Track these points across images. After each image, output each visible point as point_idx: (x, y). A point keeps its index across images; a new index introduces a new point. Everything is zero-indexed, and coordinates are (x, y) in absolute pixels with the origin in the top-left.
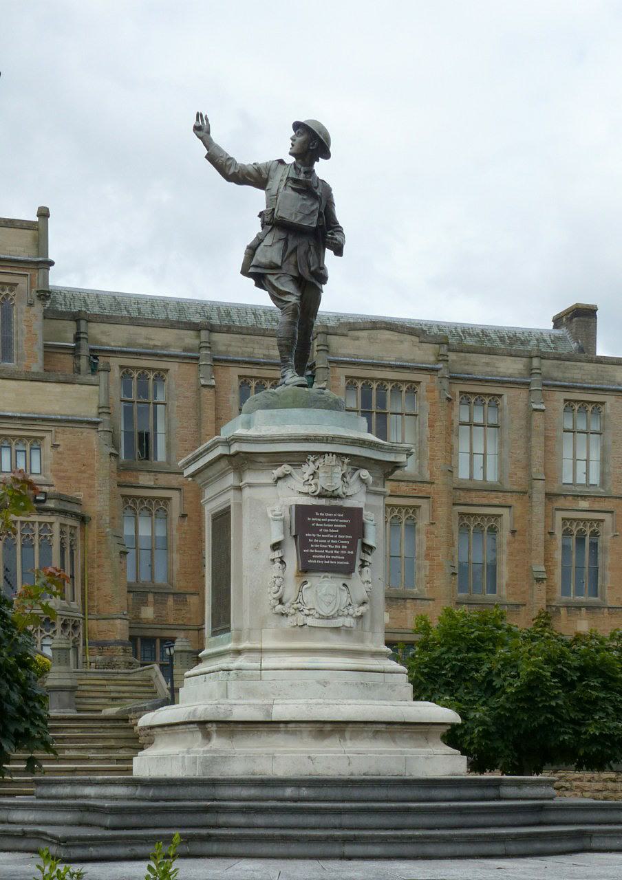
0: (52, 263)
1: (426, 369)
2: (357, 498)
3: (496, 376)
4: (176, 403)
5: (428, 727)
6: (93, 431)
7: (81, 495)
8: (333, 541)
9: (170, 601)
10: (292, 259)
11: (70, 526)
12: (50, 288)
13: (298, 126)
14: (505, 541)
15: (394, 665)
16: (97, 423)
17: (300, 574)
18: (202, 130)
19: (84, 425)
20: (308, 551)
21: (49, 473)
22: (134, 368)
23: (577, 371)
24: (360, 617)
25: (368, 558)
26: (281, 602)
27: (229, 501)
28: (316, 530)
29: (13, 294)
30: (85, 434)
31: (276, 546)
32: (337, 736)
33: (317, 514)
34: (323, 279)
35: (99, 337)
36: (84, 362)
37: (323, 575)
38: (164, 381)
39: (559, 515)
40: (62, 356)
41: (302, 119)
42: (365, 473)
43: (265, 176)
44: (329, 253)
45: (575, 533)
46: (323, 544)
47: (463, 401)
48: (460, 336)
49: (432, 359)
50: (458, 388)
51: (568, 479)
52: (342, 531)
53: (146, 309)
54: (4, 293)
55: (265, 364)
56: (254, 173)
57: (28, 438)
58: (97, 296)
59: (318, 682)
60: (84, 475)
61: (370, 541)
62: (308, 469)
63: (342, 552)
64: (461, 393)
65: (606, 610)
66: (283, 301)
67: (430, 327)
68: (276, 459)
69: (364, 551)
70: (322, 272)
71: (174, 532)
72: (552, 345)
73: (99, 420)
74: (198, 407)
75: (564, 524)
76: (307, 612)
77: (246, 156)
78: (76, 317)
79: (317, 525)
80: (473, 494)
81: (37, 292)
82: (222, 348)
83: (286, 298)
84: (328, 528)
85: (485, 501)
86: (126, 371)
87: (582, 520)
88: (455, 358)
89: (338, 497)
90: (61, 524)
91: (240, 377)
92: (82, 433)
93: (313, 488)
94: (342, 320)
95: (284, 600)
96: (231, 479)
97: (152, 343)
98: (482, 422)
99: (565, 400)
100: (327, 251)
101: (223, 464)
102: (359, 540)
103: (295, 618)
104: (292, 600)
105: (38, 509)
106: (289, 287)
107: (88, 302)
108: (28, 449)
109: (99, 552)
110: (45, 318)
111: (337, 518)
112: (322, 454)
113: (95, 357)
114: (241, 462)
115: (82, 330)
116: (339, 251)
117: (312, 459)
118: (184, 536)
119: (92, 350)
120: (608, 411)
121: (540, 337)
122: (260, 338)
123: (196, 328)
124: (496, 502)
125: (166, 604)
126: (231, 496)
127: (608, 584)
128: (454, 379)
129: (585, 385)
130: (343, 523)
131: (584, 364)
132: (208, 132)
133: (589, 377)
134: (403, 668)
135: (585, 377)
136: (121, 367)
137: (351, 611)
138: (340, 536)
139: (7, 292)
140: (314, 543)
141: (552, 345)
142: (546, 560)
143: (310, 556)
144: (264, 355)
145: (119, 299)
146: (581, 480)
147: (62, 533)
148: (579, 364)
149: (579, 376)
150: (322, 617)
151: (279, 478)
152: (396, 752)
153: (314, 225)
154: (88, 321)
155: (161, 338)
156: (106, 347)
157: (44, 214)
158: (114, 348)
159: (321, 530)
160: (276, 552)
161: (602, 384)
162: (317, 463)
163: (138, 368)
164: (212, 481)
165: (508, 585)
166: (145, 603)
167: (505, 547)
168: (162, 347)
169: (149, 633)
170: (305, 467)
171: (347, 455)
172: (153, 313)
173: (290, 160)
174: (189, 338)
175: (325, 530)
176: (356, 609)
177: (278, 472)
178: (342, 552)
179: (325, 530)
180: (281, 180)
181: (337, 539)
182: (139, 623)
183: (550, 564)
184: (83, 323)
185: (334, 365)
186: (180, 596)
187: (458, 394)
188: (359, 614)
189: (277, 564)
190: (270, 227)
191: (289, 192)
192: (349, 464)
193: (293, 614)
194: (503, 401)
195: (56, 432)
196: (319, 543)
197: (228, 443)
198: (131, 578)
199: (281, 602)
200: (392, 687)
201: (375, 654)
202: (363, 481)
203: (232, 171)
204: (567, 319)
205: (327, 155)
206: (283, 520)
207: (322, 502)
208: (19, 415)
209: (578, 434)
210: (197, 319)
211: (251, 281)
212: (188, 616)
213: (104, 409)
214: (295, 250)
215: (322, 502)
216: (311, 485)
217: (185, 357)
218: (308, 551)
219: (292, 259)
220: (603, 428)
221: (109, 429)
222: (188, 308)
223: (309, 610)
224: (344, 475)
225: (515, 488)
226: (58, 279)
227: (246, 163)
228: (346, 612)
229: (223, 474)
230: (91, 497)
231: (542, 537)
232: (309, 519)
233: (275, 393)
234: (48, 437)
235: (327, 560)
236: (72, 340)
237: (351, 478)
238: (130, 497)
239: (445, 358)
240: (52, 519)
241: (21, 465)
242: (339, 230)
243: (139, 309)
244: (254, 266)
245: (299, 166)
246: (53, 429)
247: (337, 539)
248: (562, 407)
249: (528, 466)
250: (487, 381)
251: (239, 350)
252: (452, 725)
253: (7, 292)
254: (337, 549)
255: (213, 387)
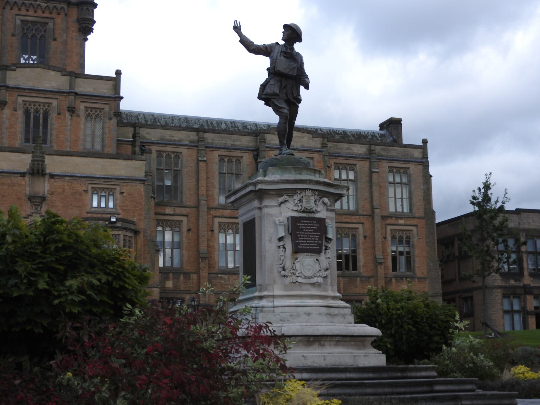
0: (122, 98)
1: (317, 151)
2: (322, 213)
3: (353, 155)
4: (186, 170)
5: (365, 338)
6: (142, 185)
7: (135, 219)
8: (311, 236)
9: (182, 277)
10: (284, 91)
11: (129, 236)
12: (121, 111)
13: (286, 27)
14: (361, 242)
15: (343, 304)
16: (144, 181)
17: (294, 254)
18: (237, 29)
19: (138, 182)
20: (297, 241)
21: (118, 208)
22: (163, 151)
23: (393, 152)
24: (325, 277)
25: (329, 245)
26: (284, 269)
27: (254, 215)
28: (302, 230)
29: (101, 114)
30: (138, 187)
31: (281, 239)
32: (317, 344)
33: (302, 221)
34: (299, 101)
35: (146, 135)
36: (137, 149)
37: (305, 254)
38: (179, 158)
39: (389, 228)
40: (126, 146)
41: (288, 23)
42: (326, 200)
43: (269, 50)
44: (302, 88)
45: (398, 237)
46: (306, 237)
47: (336, 168)
48: (332, 134)
49: (319, 146)
50: (332, 161)
51: (392, 209)
52: (315, 231)
53: (169, 121)
54: (97, 113)
55: (233, 149)
56: (264, 49)
57: (107, 189)
58: (144, 115)
59: (305, 313)
60: (137, 208)
61: (330, 236)
62: (297, 198)
63: (315, 242)
64: (334, 163)
65: (416, 279)
66: (280, 112)
67: (317, 129)
68: (279, 193)
69: (326, 241)
70: (299, 97)
71: (184, 239)
72: (380, 139)
73: (145, 179)
74: (197, 172)
75: (392, 233)
76: (298, 275)
77: (258, 41)
78: (134, 125)
79: (302, 227)
80: (343, 217)
81: (114, 112)
82: (210, 141)
83: (282, 110)
84: (308, 229)
85: (349, 221)
86: (159, 154)
87: (401, 230)
88: (331, 145)
89: (313, 212)
90: (124, 235)
91: (219, 156)
92: (136, 186)
93: (300, 208)
94: (271, 127)
95: (285, 268)
96: (256, 203)
97: (173, 138)
98: (346, 178)
99: (389, 167)
100: (301, 86)
101: (251, 196)
102: (324, 235)
103: (291, 278)
104: (290, 268)
105: (111, 227)
106: (284, 105)
107: (139, 118)
108: (107, 195)
109: (144, 250)
110: (117, 126)
111: (312, 223)
112: (304, 190)
113: (143, 146)
114: (261, 195)
115: (137, 132)
116: (307, 87)
117: (299, 192)
118: (189, 241)
119: (141, 142)
120: (411, 172)
121: (373, 135)
122: (230, 135)
123: (197, 130)
124: (355, 221)
125: (179, 279)
126: (256, 213)
127: (417, 265)
128: (331, 156)
129: (398, 159)
130: (316, 226)
131: (398, 148)
132: (240, 30)
133: (401, 155)
134: (348, 305)
135: (398, 155)
136: (157, 151)
137: (321, 274)
138: (314, 233)
139: (98, 112)
140: (301, 237)
141: (380, 139)
142: (383, 252)
143: (299, 244)
144: (232, 144)
145: (155, 116)
146: (399, 209)
147: (124, 240)
148: (395, 148)
149: (395, 154)
150: (306, 277)
151: (282, 203)
152: (349, 353)
153: (295, 74)
154: (140, 128)
155: (178, 135)
156: (149, 141)
157: (118, 73)
158: (153, 141)
159: (304, 230)
160: (281, 242)
161: (407, 158)
162: (302, 195)
163: (166, 152)
164: (243, 205)
165: (363, 266)
166: (168, 279)
167: (361, 246)
168: (179, 141)
169: (170, 296)
170: (295, 197)
171: (317, 190)
172: (173, 123)
173: (282, 43)
174: (193, 136)
175: (306, 230)
176: (323, 273)
177: (281, 199)
178: (315, 242)
179: (306, 230)
180: (278, 52)
181: (313, 235)
182: (164, 290)
183: (385, 254)
184: (137, 128)
185: (269, 149)
186: (187, 275)
187: (333, 164)
188: (325, 276)
189: (282, 249)
190: (272, 76)
191: (282, 58)
192: (318, 195)
193: (290, 276)
194: (356, 168)
195: (122, 186)
196: (303, 237)
197: (255, 184)
198: (161, 264)
199: (284, 269)
200: (344, 316)
201: (334, 298)
202: (325, 204)
203: (252, 48)
204: (387, 125)
205: (300, 40)
206: (284, 225)
207: (304, 215)
208: (103, 177)
209: (396, 185)
210: (196, 126)
211: (263, 102)
212: (192, 285)
213: (147, 174)
214: (285, 87)
215: (304, 215)
216: (299, 206)
217: (190, 146)
218: (297, 241)
219: (284, 91)
220: (409, 181)
221: (150, 184)
222: (191, 121)
223: (299, 273)
224: (315, 201)
225: (365, 213)
226: (125, 106)
227: (259, 44)
228: (318, 274)
229: (251, 201)
230: (140, 220)
231: (381, 240)
232: (298, 224)
233: (277, 159)
234: (118, 188)
235: (308, 246)
236: (131, 137)
237: (319, 202)
238: (160, 220)
239: (326, 145)
240: (120, 232)
241: (103, 205)
242: (307, 77)
243: (166, 121)
244: (265, 94)
245: (287, 45)
246: (121, 184)
247: (313, 235)
248: (388, 171)
249: (371, 202)
250: (348, 157)
251: (219, 142)
252: (377, 336)
253: (98, 112)
254: (313, 240)
255: (205, 161)
